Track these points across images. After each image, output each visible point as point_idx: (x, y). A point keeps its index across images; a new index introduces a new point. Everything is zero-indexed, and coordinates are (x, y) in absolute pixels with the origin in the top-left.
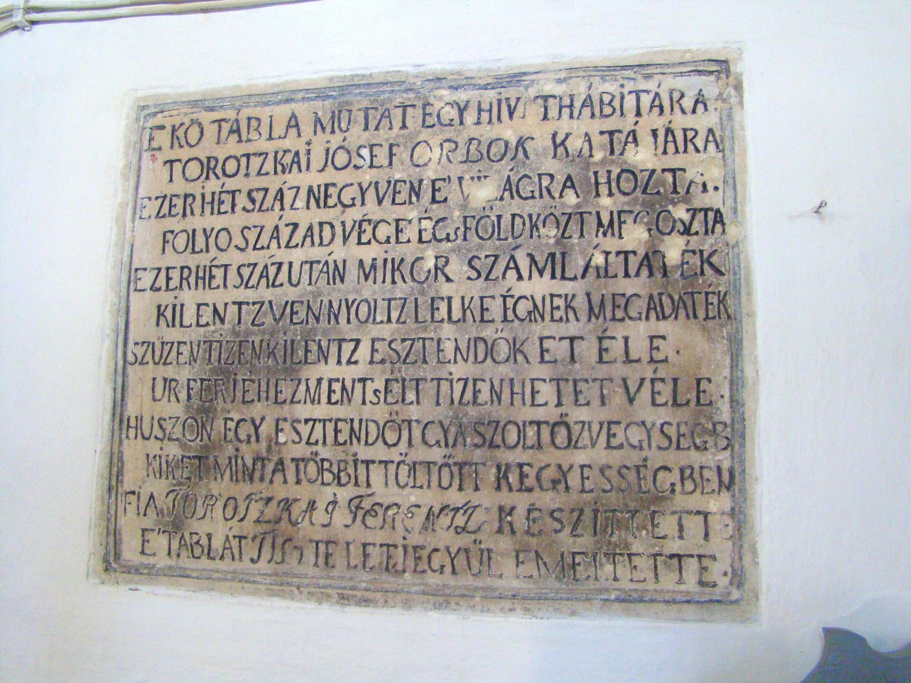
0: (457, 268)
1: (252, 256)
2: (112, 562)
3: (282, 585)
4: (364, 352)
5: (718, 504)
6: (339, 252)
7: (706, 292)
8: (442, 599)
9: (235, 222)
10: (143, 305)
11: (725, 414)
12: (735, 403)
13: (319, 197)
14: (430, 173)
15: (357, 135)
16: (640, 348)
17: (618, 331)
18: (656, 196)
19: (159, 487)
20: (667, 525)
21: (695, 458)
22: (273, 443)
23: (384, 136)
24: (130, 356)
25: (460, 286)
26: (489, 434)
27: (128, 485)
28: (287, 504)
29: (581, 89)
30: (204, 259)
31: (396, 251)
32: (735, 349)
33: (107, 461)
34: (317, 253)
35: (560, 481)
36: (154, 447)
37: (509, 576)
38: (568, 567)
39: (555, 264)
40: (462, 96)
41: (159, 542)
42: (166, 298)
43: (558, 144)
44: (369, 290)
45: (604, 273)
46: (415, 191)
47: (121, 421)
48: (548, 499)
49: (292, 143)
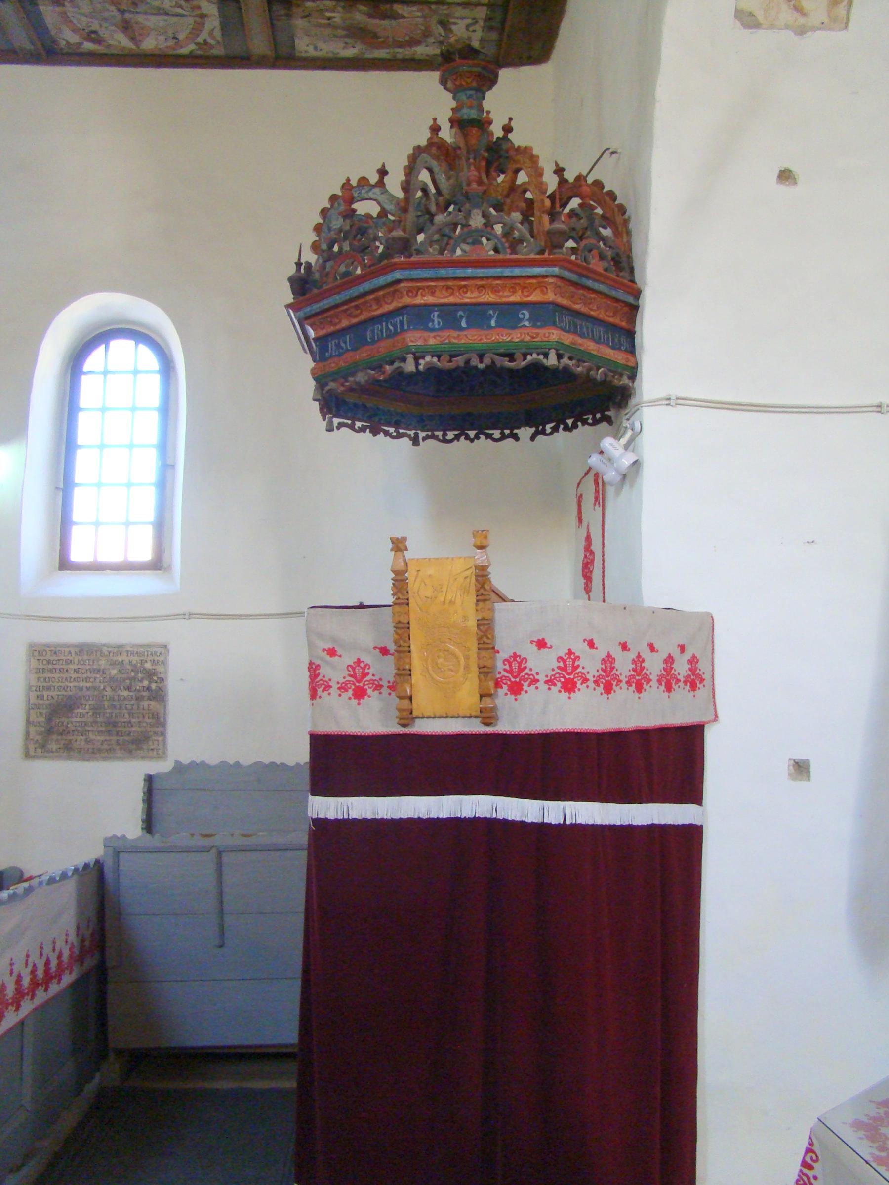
0: (108, 689)
1: (60, 684)
2: (27, 756)
3: (69, 758)
4: (87, 707)
5: (160, 738)
6: (81, 684)
8: (105, 759)
9: (57, 676)
10: (33, 695)
11: (162, 720)
12: (165, 719)
13: (76, 671)
14: (103, 667)
15: (85, 657)
16: (146, 706)
17: (142, 703)
18: (150, 675)
19: (38, 737)
20: (151, 743)
21: (156, 729)
22: (67, 727)
23: (92, 657)
24: (30, 708)
25: (109, 692)
26: (115, 725)
27: (31, 737)
28: (70, 740)
29: (136, 650)
30: (48, 684)
31: (95, 684)
32: (165, 707)
34: (76, 684)
35: (129, 734)
36: (38, 729)
37: (119, 754)
38: (130, 752)
39: (129, 689)
40: (110, 649)
41: (39, 750)
42: (39, 693)
43: (130, 662)
44: (89, 693)
45: (139, 691)
46: (99, 671)
47: (28, 722)
48: (127, 738)
49: (69, 657)
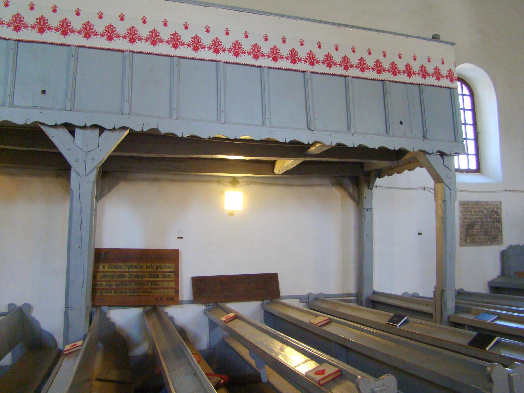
6: (476, 217)
7: (499, 221)
8: (485, 245)
13: (474, 212)
25: (484, 220)
33: (275, 314)
37: (489, 243)
39: (490, 218)
